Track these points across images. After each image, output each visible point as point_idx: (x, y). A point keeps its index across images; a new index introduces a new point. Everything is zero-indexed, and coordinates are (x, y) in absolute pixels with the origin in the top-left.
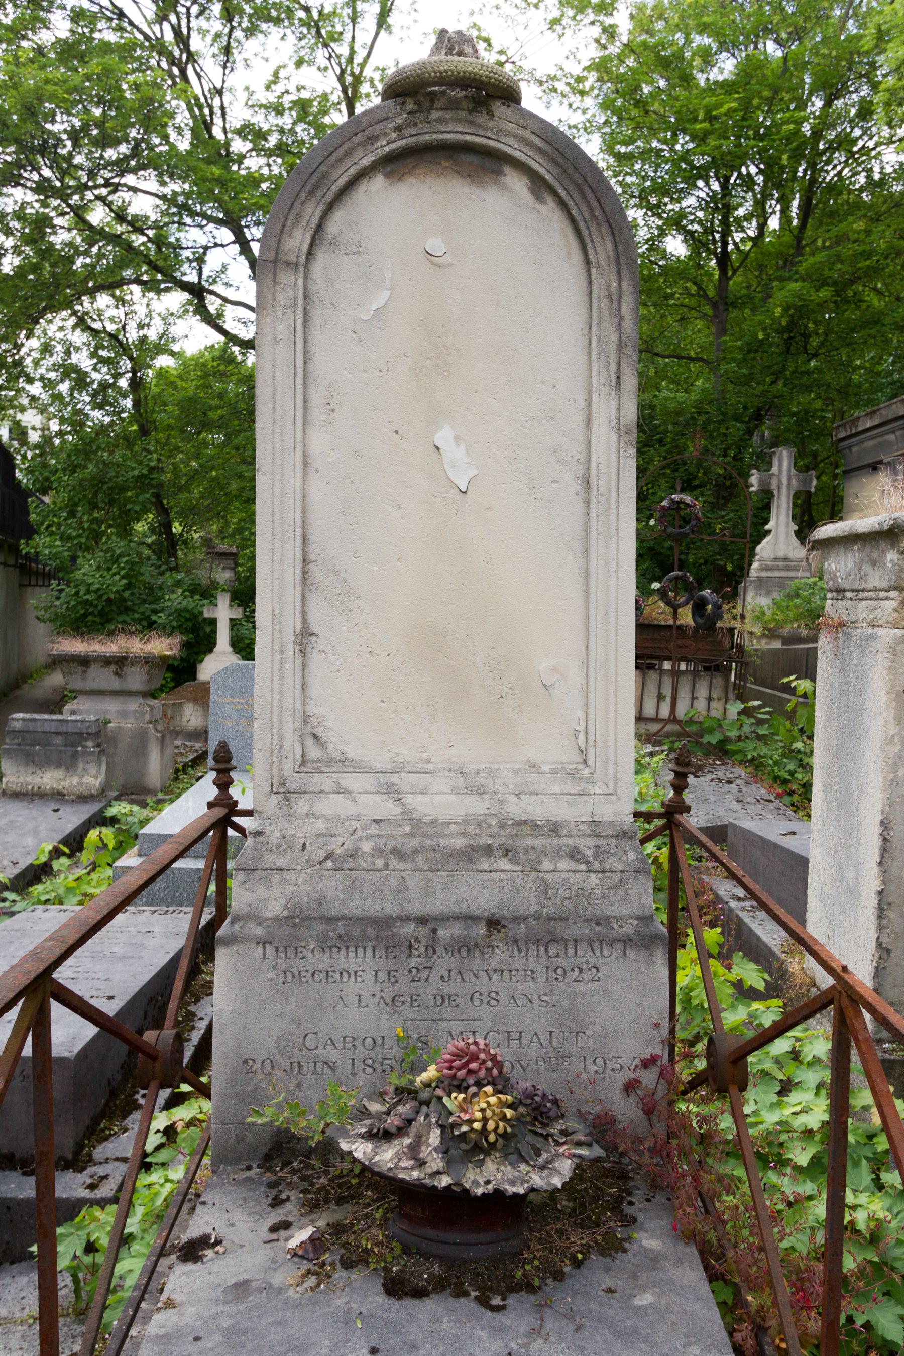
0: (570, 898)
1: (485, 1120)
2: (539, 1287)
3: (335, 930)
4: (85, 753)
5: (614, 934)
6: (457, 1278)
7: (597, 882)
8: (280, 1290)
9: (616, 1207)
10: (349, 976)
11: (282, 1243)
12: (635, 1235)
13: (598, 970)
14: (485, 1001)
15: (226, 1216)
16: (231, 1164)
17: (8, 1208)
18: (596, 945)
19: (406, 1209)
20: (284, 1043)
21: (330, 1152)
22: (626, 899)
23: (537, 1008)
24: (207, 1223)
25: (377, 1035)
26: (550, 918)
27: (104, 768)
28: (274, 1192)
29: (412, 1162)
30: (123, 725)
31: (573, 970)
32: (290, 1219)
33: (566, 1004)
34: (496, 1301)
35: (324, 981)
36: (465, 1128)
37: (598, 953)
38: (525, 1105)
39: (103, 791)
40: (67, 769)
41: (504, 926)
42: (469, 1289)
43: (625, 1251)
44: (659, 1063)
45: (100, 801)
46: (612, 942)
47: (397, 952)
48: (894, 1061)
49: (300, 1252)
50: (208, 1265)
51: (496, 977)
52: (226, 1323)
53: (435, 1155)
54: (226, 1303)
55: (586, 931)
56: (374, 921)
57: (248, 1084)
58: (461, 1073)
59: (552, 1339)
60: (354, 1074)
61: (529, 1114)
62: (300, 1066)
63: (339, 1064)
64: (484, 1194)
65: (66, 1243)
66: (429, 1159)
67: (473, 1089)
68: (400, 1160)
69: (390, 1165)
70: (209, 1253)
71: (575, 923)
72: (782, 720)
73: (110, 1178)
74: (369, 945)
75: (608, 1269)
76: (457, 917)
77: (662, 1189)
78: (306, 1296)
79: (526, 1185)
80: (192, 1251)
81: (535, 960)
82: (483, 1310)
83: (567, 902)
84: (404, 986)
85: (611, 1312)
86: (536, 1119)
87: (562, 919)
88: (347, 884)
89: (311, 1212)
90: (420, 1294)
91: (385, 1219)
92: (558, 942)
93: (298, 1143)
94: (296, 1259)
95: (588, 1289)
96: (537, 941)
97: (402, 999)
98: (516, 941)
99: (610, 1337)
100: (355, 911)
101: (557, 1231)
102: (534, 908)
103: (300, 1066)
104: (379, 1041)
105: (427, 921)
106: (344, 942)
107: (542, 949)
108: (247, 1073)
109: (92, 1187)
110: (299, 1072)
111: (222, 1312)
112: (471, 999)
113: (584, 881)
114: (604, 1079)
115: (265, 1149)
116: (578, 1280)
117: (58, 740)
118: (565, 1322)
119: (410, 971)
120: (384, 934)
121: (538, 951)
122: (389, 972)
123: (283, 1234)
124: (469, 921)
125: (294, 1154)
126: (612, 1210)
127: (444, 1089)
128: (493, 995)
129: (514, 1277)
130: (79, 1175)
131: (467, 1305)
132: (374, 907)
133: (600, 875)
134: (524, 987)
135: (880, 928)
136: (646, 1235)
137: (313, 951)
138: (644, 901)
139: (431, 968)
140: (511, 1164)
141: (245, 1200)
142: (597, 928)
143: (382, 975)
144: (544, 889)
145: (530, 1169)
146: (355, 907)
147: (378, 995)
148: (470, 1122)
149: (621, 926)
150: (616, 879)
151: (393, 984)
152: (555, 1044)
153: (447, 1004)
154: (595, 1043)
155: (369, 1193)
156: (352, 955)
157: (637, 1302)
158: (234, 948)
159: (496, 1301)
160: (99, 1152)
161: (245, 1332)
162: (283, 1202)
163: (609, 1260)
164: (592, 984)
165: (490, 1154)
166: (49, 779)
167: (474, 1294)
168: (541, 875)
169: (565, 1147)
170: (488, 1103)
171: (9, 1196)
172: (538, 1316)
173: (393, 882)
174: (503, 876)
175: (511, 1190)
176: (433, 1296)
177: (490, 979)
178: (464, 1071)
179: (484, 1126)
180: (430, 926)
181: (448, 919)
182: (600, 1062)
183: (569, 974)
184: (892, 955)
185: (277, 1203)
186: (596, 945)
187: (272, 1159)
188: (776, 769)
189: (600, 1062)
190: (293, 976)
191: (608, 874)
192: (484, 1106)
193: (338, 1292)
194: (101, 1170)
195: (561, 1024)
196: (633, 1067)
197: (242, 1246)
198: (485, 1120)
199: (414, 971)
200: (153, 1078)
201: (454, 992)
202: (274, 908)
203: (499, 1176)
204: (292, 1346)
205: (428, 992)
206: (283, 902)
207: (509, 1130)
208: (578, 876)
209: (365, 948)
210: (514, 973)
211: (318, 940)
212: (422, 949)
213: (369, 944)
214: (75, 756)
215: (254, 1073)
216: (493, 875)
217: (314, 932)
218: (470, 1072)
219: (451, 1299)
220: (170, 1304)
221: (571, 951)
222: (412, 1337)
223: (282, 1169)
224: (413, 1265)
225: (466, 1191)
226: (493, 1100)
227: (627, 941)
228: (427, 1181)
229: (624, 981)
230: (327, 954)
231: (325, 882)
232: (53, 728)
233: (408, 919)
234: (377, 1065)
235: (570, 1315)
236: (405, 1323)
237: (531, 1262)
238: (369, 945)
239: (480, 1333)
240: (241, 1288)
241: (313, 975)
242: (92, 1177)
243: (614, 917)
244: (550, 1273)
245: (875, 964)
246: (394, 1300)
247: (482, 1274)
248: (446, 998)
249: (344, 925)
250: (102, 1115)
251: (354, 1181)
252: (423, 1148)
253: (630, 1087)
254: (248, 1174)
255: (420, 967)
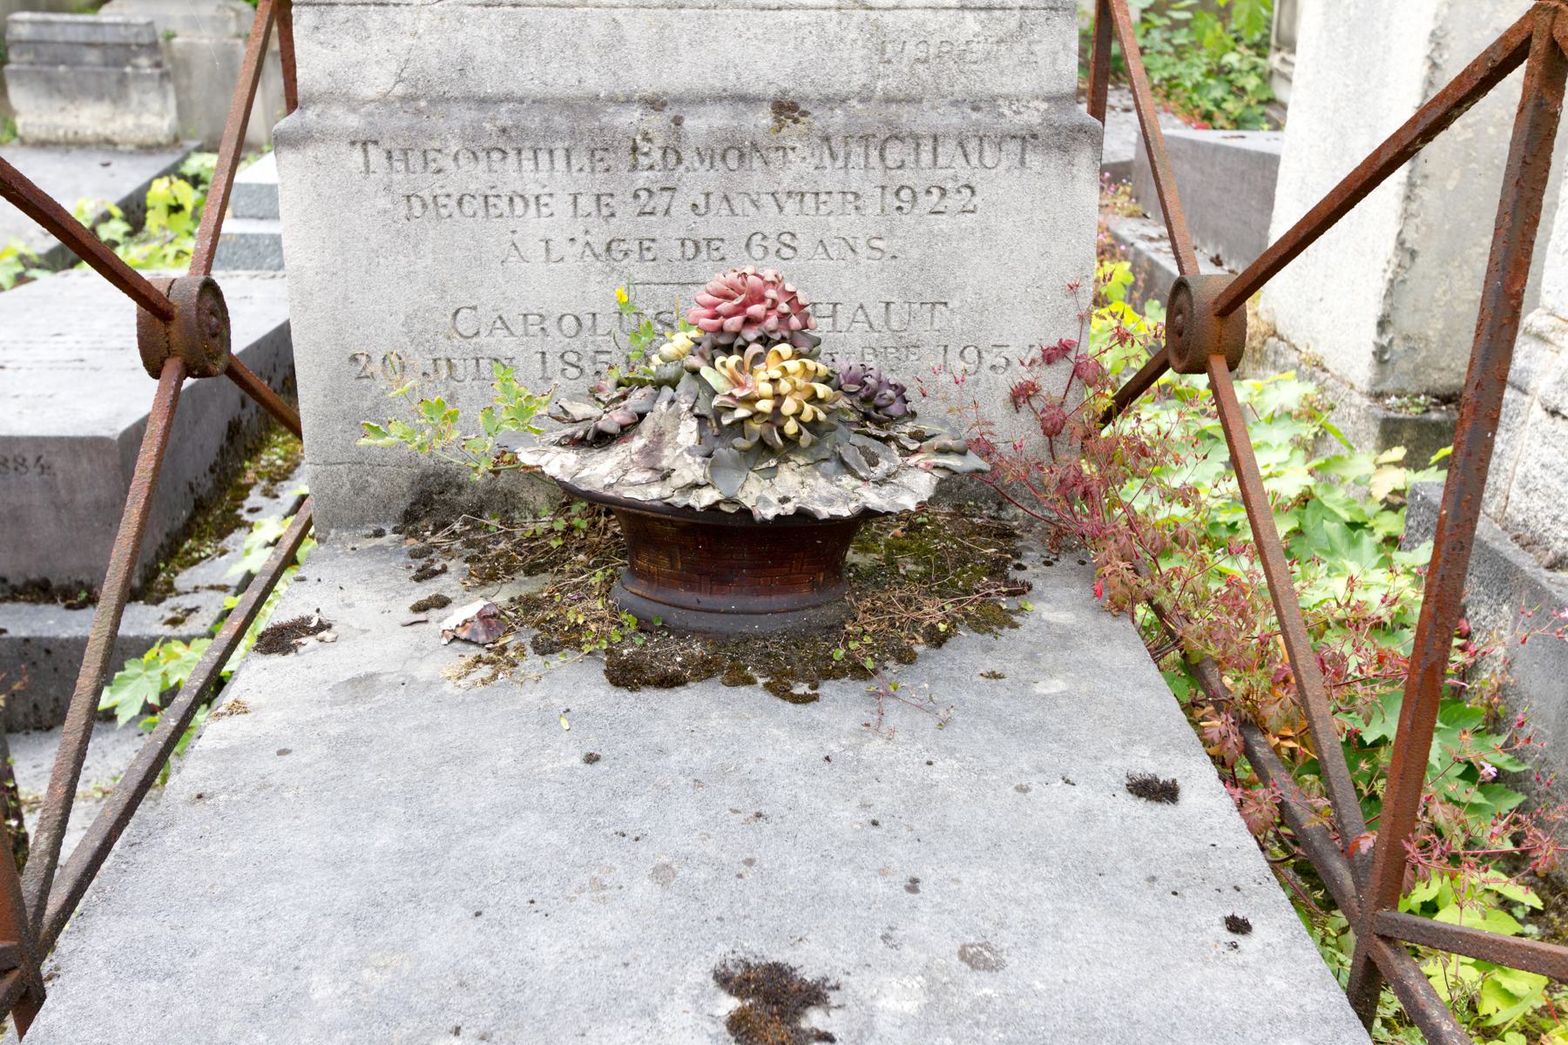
0: (926, 61)
1: (779, 398)
2: (875, 672)
3: (494, 119)
4: (138, 77)
5: (1004, 125)
6: (733, 660)
7: (978, 28)
8: (429, 685)
9: (996, 569)
10: (527, 205)
11: (432, 626)
12: (1030, 607)
13: (973, 192)
14: (772, 250)
15: (341, 594)
16: (348, 528)
17: (48, 652)
18: (972, 145)
19: (643, 563)
20: (418, 327)
21: (515, 507)
22: (1028, 62)
23: (864, 261)
24: (306, 604)
25: (583, 311)
26: (888, 100)
27: (172, 102)
28: (422, 562)
29: (648, 475)
30: (195, 40)
31: (928, 192)
32: (448, 594)
33: (915, 253)
34: (801, 689)
35: (481, 213)
36: (742, 412)
37: (974, 159)
38: (849, 394)
39: (176, 140)
40: (114, 101)
41: (805, 114)
42: (755, 674)
43: (1015, 626)
44: (1072, 355)
45: (172, 152)
46: (1001, 140)
47: (610, 159)
48: (1403, 421)
49: (464, 635)
50: (307, 656)
51: (790, 206)
52: (334, 730)
53: (689, 459)
54: (333, 704)
55: (955, 120)
56: (567, 105)
57: (362, 397)
58: (733, 323)
59: (899, 737)
60: (547, 379)
61: (854, 409)
62: (451, 366)
63: (519, 361)
64: (778, 516)
65: (131, 687)
66: (677, 465)
67: (755, 348)
68: (626, 472)
69: (608, 480)
70: (310, 641)
71: (933, 108)
72: (1210, 18)
73: (202, 611)
74: (559, 147)
75: (988, 649)
76: (718, 99)
77: (1070, 549)
78: (474, 690)
79: (853, 505)
80: (279, 641)
81: (863, 173)
82: (779, 701)
83: (920, 68)
84: (626, 223)
85: (996, 703)
86: (867, 417)
87: (910, 100)
88: (512, 31)
89: (483, 584)
90: (669, 682)
91: (608, 582)
92: (902, 140)
93: (459, 493)
94: (457, 645)
95: (956, 674)
96: (865, 138)
97: (624, 246)
98: (827, 139)
99: (997, 735)
100: (529, 85)
101: (901, 600)
102: (856, 84)
103: (451, 366)
104: (587, 322)
105: (664, 104)
106: (510, 142)
107: (874, 154)
108: (359, 378)
109: (174, 622)
110: (451, 376)
111: (329, 716)
112: (747, 246)
113: (952, 27)
114: (977, 383)
115: (403, 505)
116: (934, 662)
117: (92, 56)
118: (920, 716)
119: (636, 196)
120: (585, 126)
121: (867, 156)
122: (598, 197)
123: (434, 613)
124: (741, 106)
125: (454, 511)
126: (991, 574)
127: (702, 355)
128: (787, 239)
129: (831, 658)
130: (154, 608)
131: (755, 697)
132: (564, 78)
133: (983, 15)
134: (842, 223)
135: (1406, 216)
136: (1048, 606)
137: (456, 158)
138: (1060, 65)
139: (673, 189)
140: (824, 475)
141: (371, 574)
142: (975, 116)
143: (587, 203)
144: (879, 42)
145: (860, 483)
146: (529, 78)
147: (581, 240)
148: (750, 401)
149: (1017, 113)
150: (1012, 22)
151: (606, 218)
152: (895, 325)
153: (704, 255)
154: (963, 322)
155: (581, 557)
156: (528, 165)
157: (1039, 689)
158: (310, 152)
159: (801, 689)
160: (183, 580)
161: (368, 741)
162: (435, 573)
163: (987, 636)
164: (962, 217)
165: (787, 460)
166: (89, 118)
167: (761, 681)
168: (873, 15)
169: (919, 457)
170: (784, 369)
171: (45, 634)
172: (875, 709)
173: (598, 29)
174: (803, 16)
175: (825, 512)
176: (691, 684)
177: (781, 209)
178: (738, 319)
179: (777, 408)
180: (670, 113)
181: (703, 101)
182: (971, 354)
183: (922, 198)
184: (1419, 260)
185: (424, 575)
186: (972, 145)
187: (417, 519)
188: (1195, 97)
189: (971, 354)
190: (424, 206)
191: (998, 13)
192: (777, 374)
193: (529, 685)
194: (187, 602)
195: (906, 290)
196: (1027, 362)
197: (364, 631)
198: (779, 398)
199: (644, 195)
200: (170, 353)
201: (716, 234)
202: (378, 81)
203: (805, 493)
204: (448, 757)
205: (669, 233)
206: (394, 67)
207: (822, 416)
208: (943, 16)
209: (551, 152)
210: (823, 197)
211: (463, 137)
212: (657, 155)
213: (559, 144)
214: (123, 81)
215: (372, 376)
216: (784, 14)
217: (456, 124)
218: (749, 322)
219: (724, 689)
220: (238, 708)
221: (926, 157)
222: (657, 739)
223: (434, 533)
224: (658, 644)
225: (747, 513)
226: (793, 365)
227: (1027, 138)
228: (679, 501)
229: (1019, 212)
230: (483, 164)
231: (469, 29)
232: (80, 35)
233: (629, 101)
234: (585, 364)
235: (927, 707)
236: (644, 721)
237: (858, 637)
238: (559, 147)
239: (775, 731)
240: (363, 684)
241: (460, 202)
242: (173, 609)
243: (1006, 97)
244: (892, 652)
245: (1389, 275)
246: (625, 692)
247: (776, 656)
248: (703, 245)
249: (511, 111)
250: (187, 531)
251: (554, 544)
252: (667, 452)
253: (1022, 395)
254: (378, 541)
255: (655, 188)
